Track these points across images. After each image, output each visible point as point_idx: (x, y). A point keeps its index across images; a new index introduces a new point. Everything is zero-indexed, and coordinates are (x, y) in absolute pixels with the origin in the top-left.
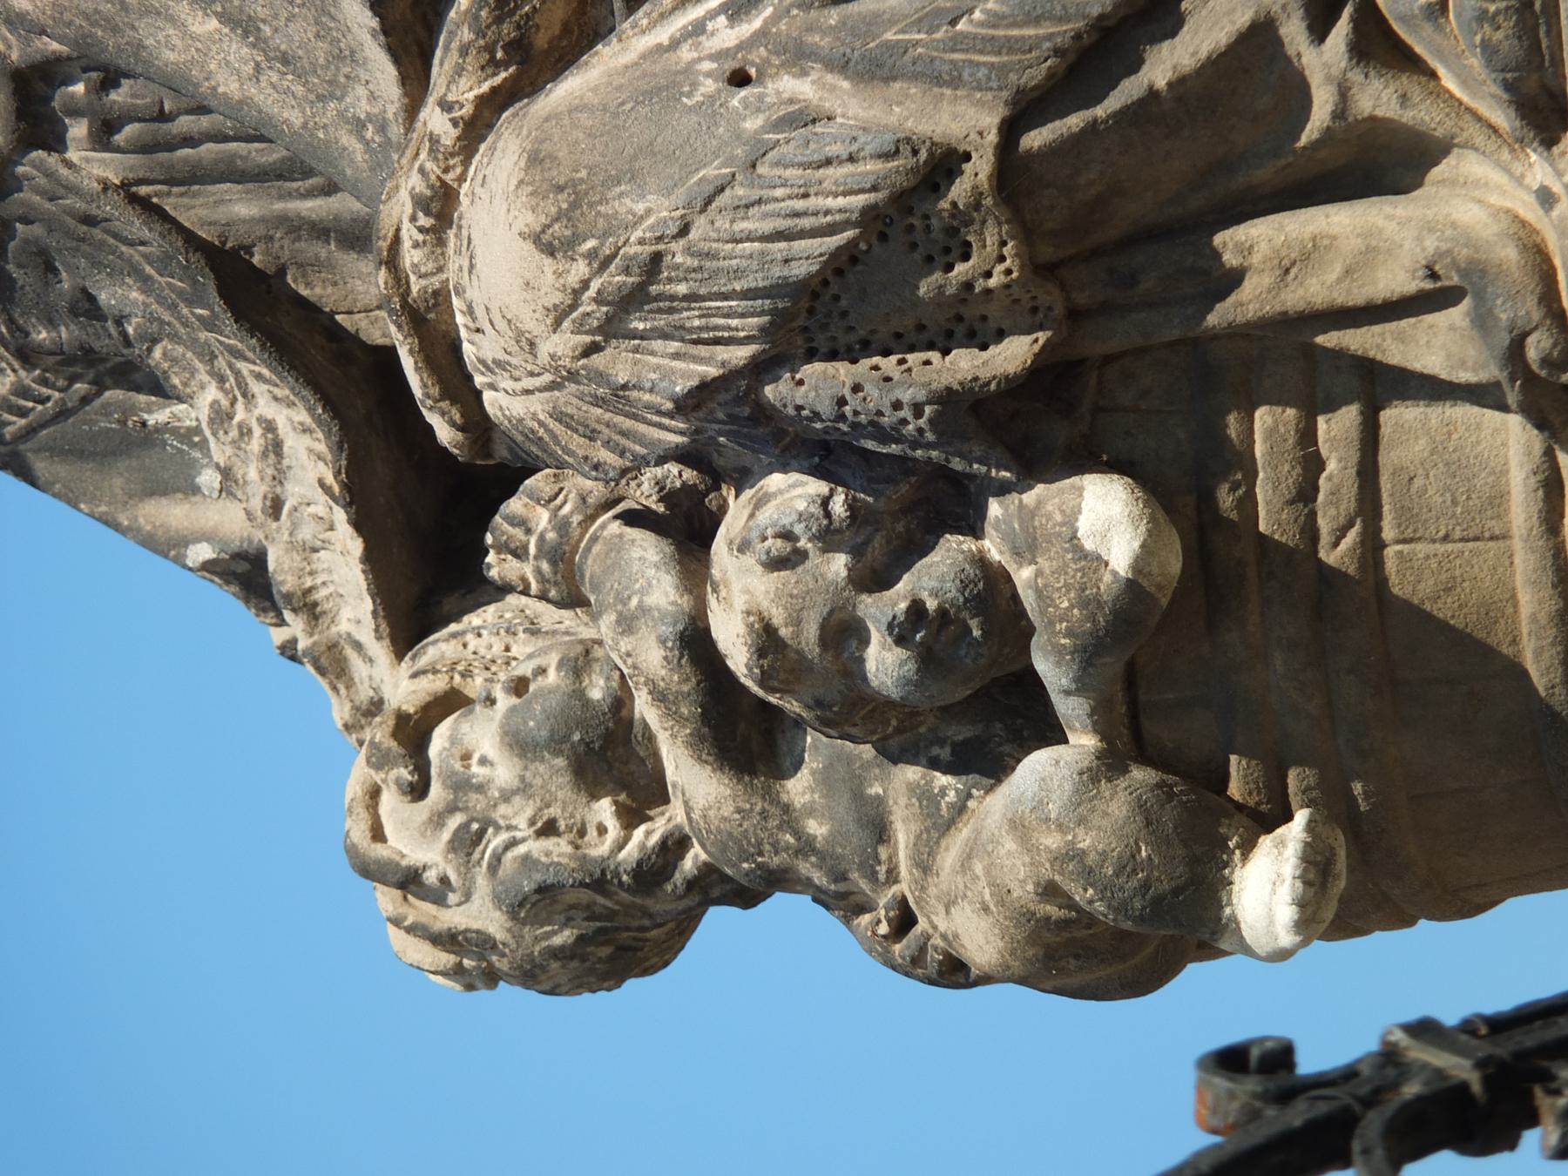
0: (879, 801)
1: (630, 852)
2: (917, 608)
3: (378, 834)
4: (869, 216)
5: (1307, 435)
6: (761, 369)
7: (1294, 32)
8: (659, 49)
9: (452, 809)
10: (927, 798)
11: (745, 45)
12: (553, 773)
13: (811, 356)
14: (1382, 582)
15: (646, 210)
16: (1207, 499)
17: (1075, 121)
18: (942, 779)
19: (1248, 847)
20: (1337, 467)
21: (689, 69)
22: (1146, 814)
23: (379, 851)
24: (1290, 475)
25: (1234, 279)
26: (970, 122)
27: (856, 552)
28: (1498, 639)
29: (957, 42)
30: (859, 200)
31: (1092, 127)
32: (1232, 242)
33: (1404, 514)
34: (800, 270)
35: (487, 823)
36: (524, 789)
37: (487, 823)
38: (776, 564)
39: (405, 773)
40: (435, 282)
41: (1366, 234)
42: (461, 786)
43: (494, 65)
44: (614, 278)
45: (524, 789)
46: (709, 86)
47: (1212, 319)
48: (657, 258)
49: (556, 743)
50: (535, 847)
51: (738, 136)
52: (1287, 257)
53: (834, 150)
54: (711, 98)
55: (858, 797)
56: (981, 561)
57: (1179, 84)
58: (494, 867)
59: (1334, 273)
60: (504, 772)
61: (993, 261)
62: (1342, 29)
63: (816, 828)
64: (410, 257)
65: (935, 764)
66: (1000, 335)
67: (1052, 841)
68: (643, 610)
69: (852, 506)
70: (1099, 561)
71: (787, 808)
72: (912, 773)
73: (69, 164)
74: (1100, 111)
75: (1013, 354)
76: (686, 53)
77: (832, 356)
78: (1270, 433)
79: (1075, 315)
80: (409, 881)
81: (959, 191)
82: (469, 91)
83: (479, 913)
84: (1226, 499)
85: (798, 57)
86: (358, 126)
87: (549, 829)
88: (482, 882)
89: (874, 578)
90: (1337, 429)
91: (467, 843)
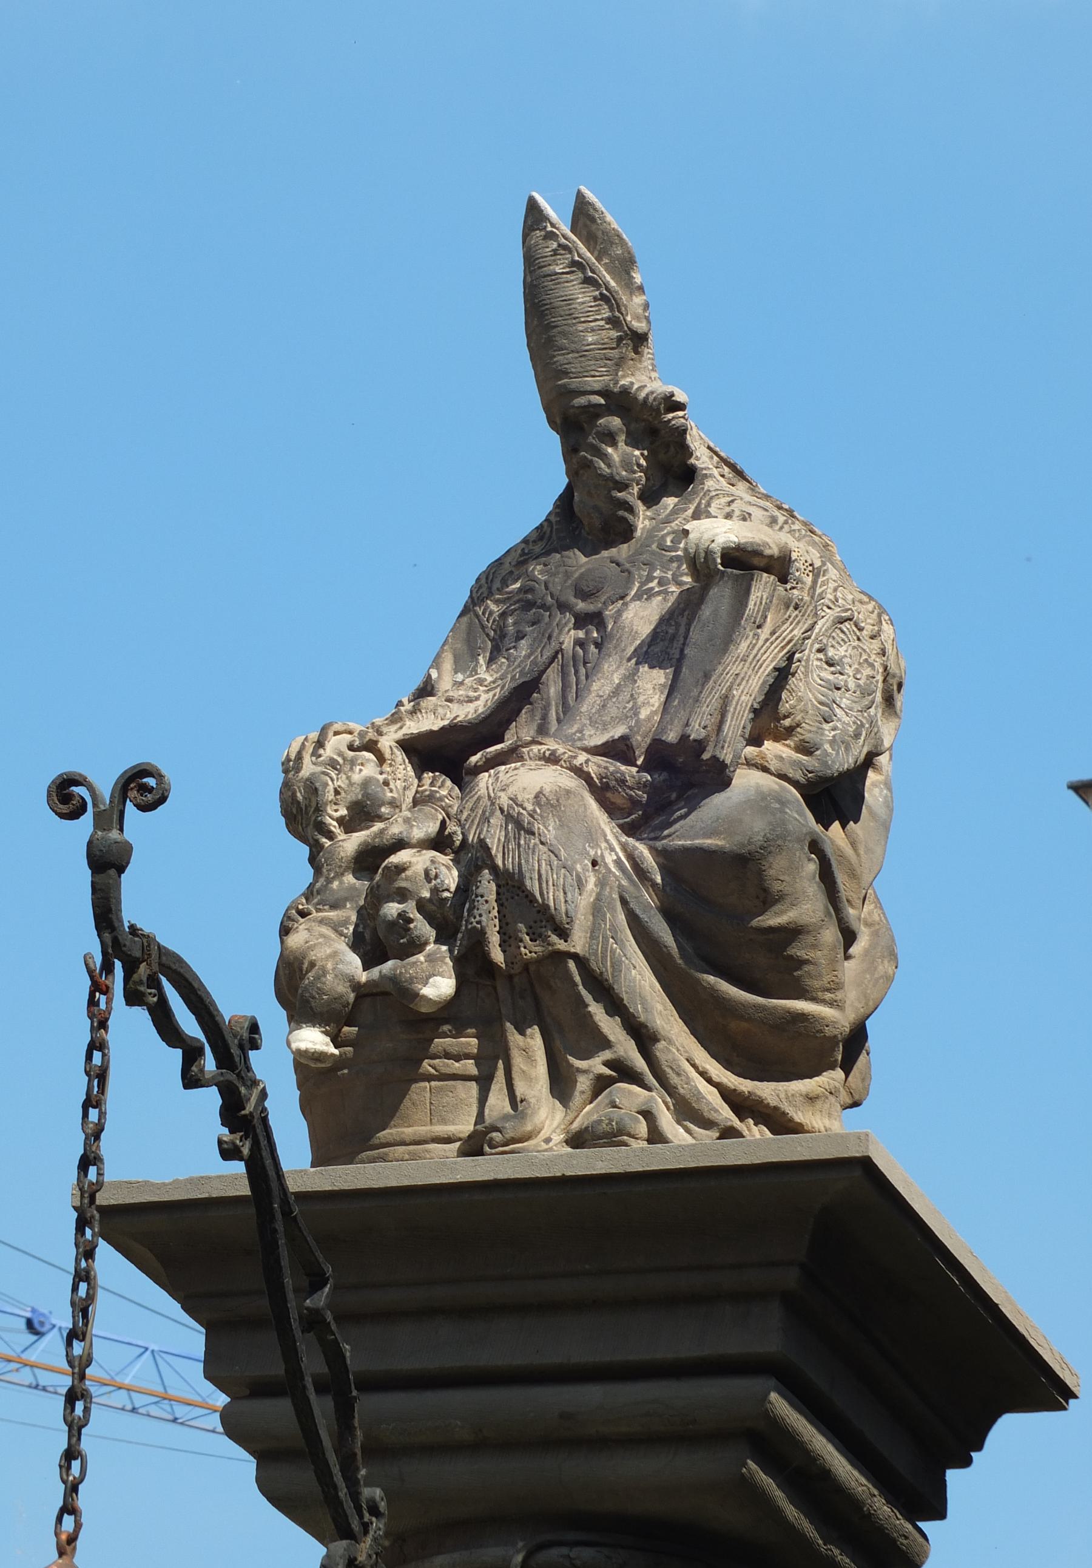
0: (344, 907)
1: (328, 820)
2: (411, 921)
3: (336, 733)
5: (467, 1056)
6: (494, 869)
7: (607, 1055)
8: (605, 836)
9: (344, 759)
10: (345, 923)
12: (356, 794)
13: (498, 886)
15: (550, 830)
16: (446, 1021)
18: (351, 928)
19: (326, 1033)
20: (456, 1066)
23: (331, 734)
24: (454, 1050)
25: (522, 1033)
26: (578, 943)
27: (430, 900)
30: (552, 904)
33: (440, 1090)
34: (528, 883)
35: (339, 771)
37: (339, 771)
40: (526, 757)
42: (353, 763)
43: (601, 778)
44: (526, 819)
45: (351, 784)
47: (508, 1024)
48: (533, 834)
49: (366, 795)
50: (331, 787)
51: (575, 862)
52: (529, 1050)
53: (569, 895)
54: (588, 853)
56: (426, 943)
57: (590, 1015)
60: (357, 777)
61: (530, 949)
62: (607, 1071)
63: (335, 884)
64: (535, 748)
65: (357, 926)
66: (504, 951)
67: (329, 966)
69: (446, 899)
70: (425, 984)
71: (342, 874)
73: (569, 631)
74: (581, 987)
75: (498, 956)
76: (604, 845)
77: (498, 894)
78: (468, 1044)
79: (510, 977)
80: (320, 744)
81: (554, 938)
82: (592, 769)
83: (308, 768)
84: (446, 1028)
85: (601, 883)
86: (581, 731)
87: (337, 792)
90: (469, 1066)
91: (333, 764)
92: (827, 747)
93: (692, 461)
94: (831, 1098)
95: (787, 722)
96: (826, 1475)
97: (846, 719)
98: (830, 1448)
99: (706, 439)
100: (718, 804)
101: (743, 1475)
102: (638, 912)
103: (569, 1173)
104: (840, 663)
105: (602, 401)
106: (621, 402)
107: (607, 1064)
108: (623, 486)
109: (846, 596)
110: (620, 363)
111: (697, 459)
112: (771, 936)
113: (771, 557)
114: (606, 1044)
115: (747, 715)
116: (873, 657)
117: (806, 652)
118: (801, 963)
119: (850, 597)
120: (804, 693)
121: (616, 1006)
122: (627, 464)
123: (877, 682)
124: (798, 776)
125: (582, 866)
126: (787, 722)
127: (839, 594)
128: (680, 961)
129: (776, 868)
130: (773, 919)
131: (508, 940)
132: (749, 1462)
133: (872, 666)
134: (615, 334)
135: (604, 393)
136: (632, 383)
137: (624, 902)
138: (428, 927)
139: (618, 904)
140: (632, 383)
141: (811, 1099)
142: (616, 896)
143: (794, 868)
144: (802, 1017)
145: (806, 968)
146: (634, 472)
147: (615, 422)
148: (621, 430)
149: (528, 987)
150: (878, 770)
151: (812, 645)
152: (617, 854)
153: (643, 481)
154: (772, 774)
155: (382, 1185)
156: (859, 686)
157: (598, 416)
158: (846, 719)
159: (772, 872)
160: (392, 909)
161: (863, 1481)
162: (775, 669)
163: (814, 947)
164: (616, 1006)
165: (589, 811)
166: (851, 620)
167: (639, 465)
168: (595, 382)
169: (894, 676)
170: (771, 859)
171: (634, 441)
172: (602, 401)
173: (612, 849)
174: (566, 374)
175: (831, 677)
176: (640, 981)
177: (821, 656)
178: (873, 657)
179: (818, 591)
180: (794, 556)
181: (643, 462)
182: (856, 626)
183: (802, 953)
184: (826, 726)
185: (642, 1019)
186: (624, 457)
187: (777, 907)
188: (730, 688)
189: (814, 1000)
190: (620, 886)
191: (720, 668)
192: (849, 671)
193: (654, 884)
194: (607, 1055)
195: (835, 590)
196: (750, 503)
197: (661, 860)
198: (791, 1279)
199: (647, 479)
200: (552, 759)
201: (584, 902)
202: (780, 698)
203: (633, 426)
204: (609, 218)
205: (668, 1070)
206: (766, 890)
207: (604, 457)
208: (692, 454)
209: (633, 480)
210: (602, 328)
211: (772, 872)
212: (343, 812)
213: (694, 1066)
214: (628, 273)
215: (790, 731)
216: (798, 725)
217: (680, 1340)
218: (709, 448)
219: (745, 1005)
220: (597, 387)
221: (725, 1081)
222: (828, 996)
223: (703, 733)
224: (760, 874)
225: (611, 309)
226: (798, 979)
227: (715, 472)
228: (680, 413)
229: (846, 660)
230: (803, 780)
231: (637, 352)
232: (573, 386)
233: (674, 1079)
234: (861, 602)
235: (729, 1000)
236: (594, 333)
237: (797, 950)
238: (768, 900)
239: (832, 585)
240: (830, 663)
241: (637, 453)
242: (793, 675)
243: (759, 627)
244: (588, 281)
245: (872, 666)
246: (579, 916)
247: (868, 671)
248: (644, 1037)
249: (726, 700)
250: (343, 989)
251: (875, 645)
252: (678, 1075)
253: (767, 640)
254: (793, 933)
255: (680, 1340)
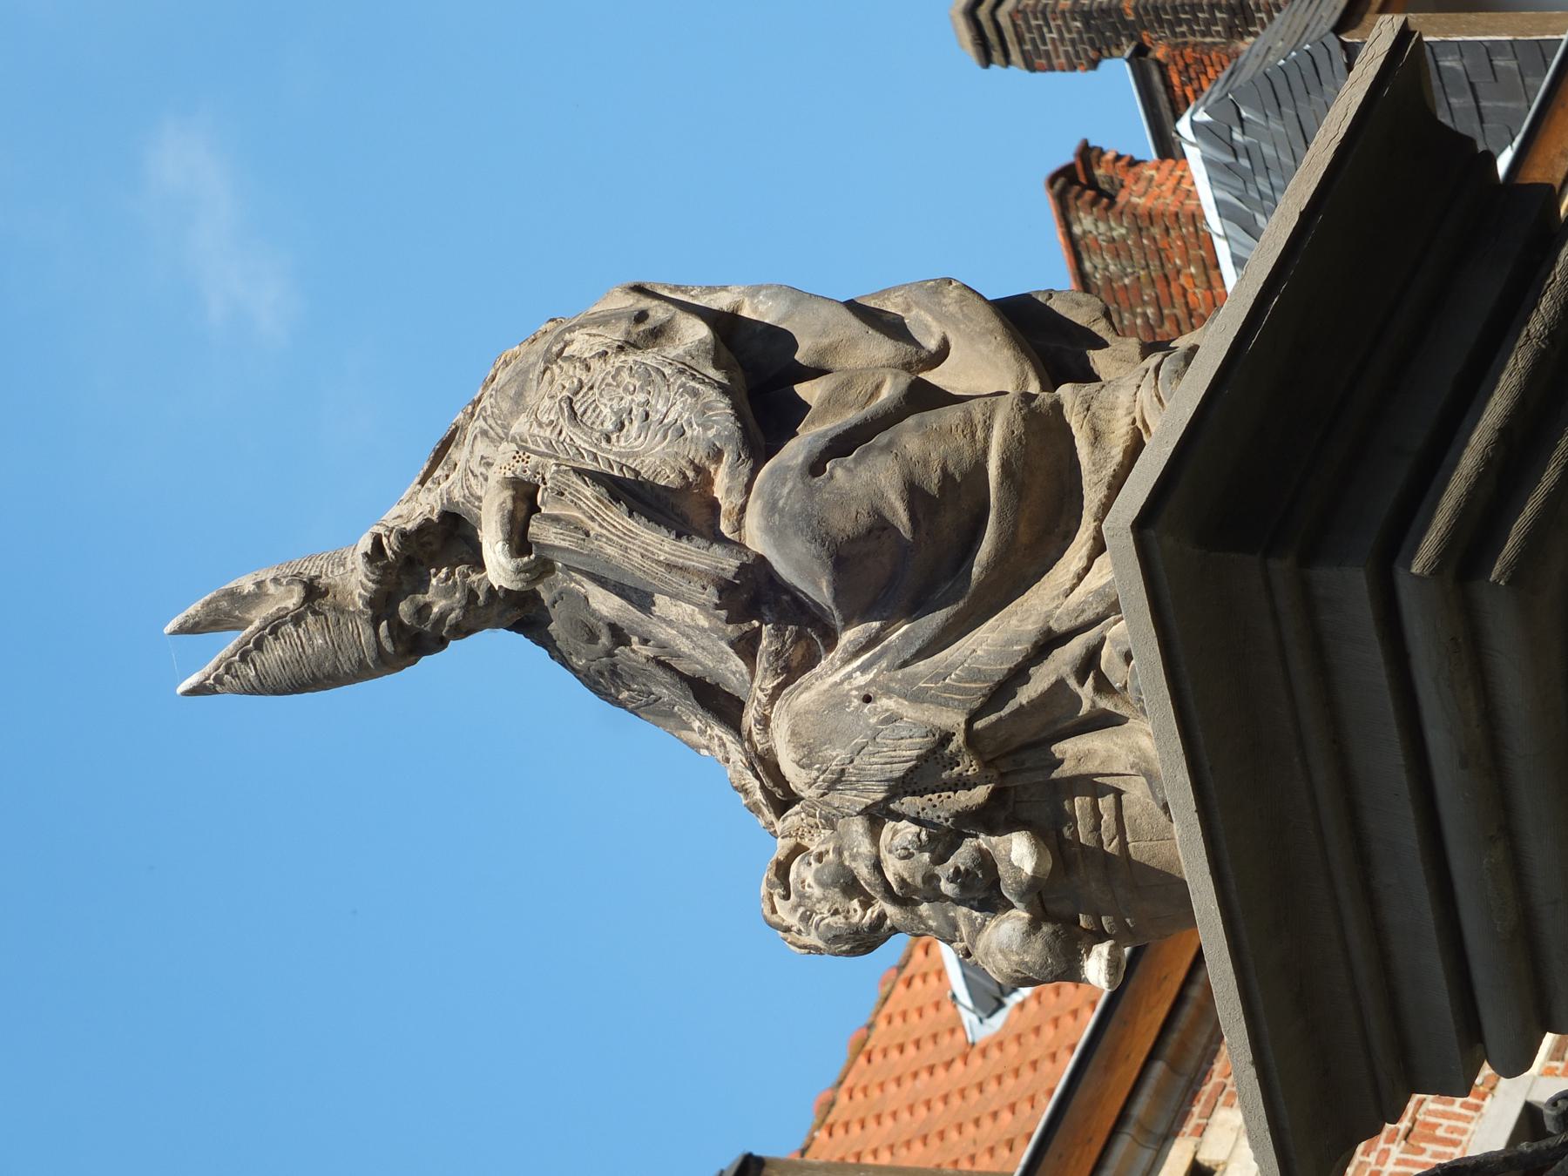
0: (954, 918)
1: (866, 920)
2: (957, 869)
3: (774, 911)
4: (918, 758)
5: (1095, 807)
6: (887, 800)
7: (1072, 683)
8: (836, 684)
9: (800, 905)
10: (972, 921)
11: (868, 684)
12: (835, 894)
13: (906, 794)
14: (1129, 856)
15: (837, 755)
16: (1060, 833)
17: (993, 717)
18: (976, 914)
19: (1089, 952)
20: (1107, 818)
21: (847, 694)
22: (1049, 947)
23: (774, 918)
24: (1090, 822)
25: (1061, 761)
26: (953, 720)
27: (932, 852)
28: (1174, 872)
29: (947, 688)
30: (915, 753)
31: (1000, 719)
32: (1059, 749)
33: (1133, 831)
34: (897, 775)
35: (813, 912)
36: (825, 898)
37: (813, 912)
38: (904, 858)
39: (781, 891)
40: (766, 746)
41: (1108, 751)
42: (802, 896)
43: (777, 675)
44: (828, 776)
45: (825, 898)
46: (856, 702)
47: (1054, 775)
48: (843, 771)
49: (834, 884)
50: (830, 920)
51: (868, 725)
52: (1077, 753)
53: (904, 734)
54: (857, 708)
55: (946, 916)
56: (979, 849)
57: (1031, 702)
58: (817, 927)
59: (1097, 763)
60: (817, 892)
61: (968, 766)
62: (1090, 681)
63: (931, 923)
64: (756, 738)
65: (972, 907)
66: (975, 785)
67: (1015, 958)
68: (859, 854)
69: (928, 835)
70: (1020, 869)
71: (920, 917)
72: (965, 910)
73: (633, 651)
74: (1002, 713)
75: (980, 793)
76: (846, 686)
77: (914, 794)
78: (1081, 807)
79: (1002, 775)
80: (788, 930)
81: (952, 747)
82: (770, 685)
83: (813, 939)
84: (1067, 833)
85: (888, 692)
86: (734, 673)
87: (836, 912)
88: (813, 929)
89: (940, 859)
90: (1106, 803)
91: (806, 918)
92: (711, 433)
93: (435, 518)
94: (1093, 409)
95: (691, 474)
96: (1505, 433)
97: (679, 406)
98: (1475, 437)
99: (409, 491)
100: (784, 569)
101: (1507, 583)
102: (913, 650)
103: (1194, 807)
104: (618, 413)
105: (384, 623)
106: (381, 606)
107: (1082, 683)
108: (472, 595)
109: (548, 409)
110: (340, 609)
111: (432, 510)
112: (920, 516)
113: (515, 499)
114: (1060, 684)
115: (684, 543)
116: (609, 368)
117: (611, 457)
118: (946, 475)
119: (547, 402)
120: (655, 459)
121: (1019, 674)
122: (448, 592)
123: (635, 362)
124: (745, 469)
125: (871, 715)
126: (691, 474)
127: (545, 420)
128: (961, 604)
129: (844, 523)
130: (900, 516)
131: (966, 784)
132: (1493, 577)
133: (619, 370)
134: (310, 618)
135: (375, 624)
136: (360, 596)
137: (905, 664)
138: (961, 850)
139: (907, 670)
140: (360, 596)
141: (1097, 437)
142: (899, 674)
143: (843, 500)
144: (1006, 466)
145: (951, 468)
146: (455, 583)
147: (404, 608)
148: (412, 601)
149: (1013, 760)
150: (739, 306)
151: (603, 450)
152: (855, 671)
153: (463, 568)
154: (746, 501)
155: (1233, 977)
156: (642, 387)
157: (401, 623)
158: (679, 406)
159: (849, 528)
160: (947, 887)
161: (1512, 361)
162: (631, 516)
163: (926, 463)
164: (1019, 674)
165: (813, 707)
166: (571, 400)
167: (447, 578)
168: (366, 634)
169: (629, 333)
170: (835, 531)
171: (423, 585)
172: (384, 623)
173: (849, 676)
174: (361, 662)
175: (636, 424)
176: (990, 643)
177: (614, 437)
178: (609, 368)
179: (543, 449)
180: (509, 474)
181: (442, 574)
182: (577, 393)
183: (935, 477)
184: (689, 433)
185: (1028, 646)
186: (439, 594)
187: (888, 514)
188: (658, 562)
189: (985, 452)
190: (888, 669)
191: (638, 573)
192: (625, 403)
193: (882, 629)
194: (1072, 683)
195: (540, 425)
196: (472, 452)
197: (855, 621)
198: (1282, 567)
199: (462, 562)
200: (765, 722)
201: (909, 711)
202: (665, 487)
203: (406, 587)
204: (191, 610)
205: (1080, 620)
206: (870, 531)
207: (443, 616)
208: (428, 520)
209: (463, 583)
210: (307, 631)
211: (849, 528)
212: (855, 903)
213: (1072, 589)
214: (245, 597)
215: (699, 470)
216: (692, 462)
217: (1364, 661)
218: (422, 483)
219: (1000, 534)
220: (370, 631)
221: (1084, 551)
222: (980, 434)
223: (711, 589)
224: (851, 541)
225: (285, 623)
226: (965, 475)
227: (444, 485)
228: (385, 541)
229: (616, 407)
230: (750, 464)
231: (327, 592)
232: (374, 654)
233: (1089, 615)
234: (552, 382)
235: (997, 550)
236: (314, 638)
237: (932, 483)
238: (880, 525)
239: (536, 430)
240: (621, 426)
241: (434, 581)
242: (637, 473)
243: (587, 534)
244: (259, 645)
245: (619, 370)
246: (925, 718)
247: (625, 374)
248: (1048, 642)
249: (670, 566)
250: (1038, 944)
251: (596, 364)
252: (1083, 611)
253: (601, 525)
254: (913, 492)
255: (1364, 661)
